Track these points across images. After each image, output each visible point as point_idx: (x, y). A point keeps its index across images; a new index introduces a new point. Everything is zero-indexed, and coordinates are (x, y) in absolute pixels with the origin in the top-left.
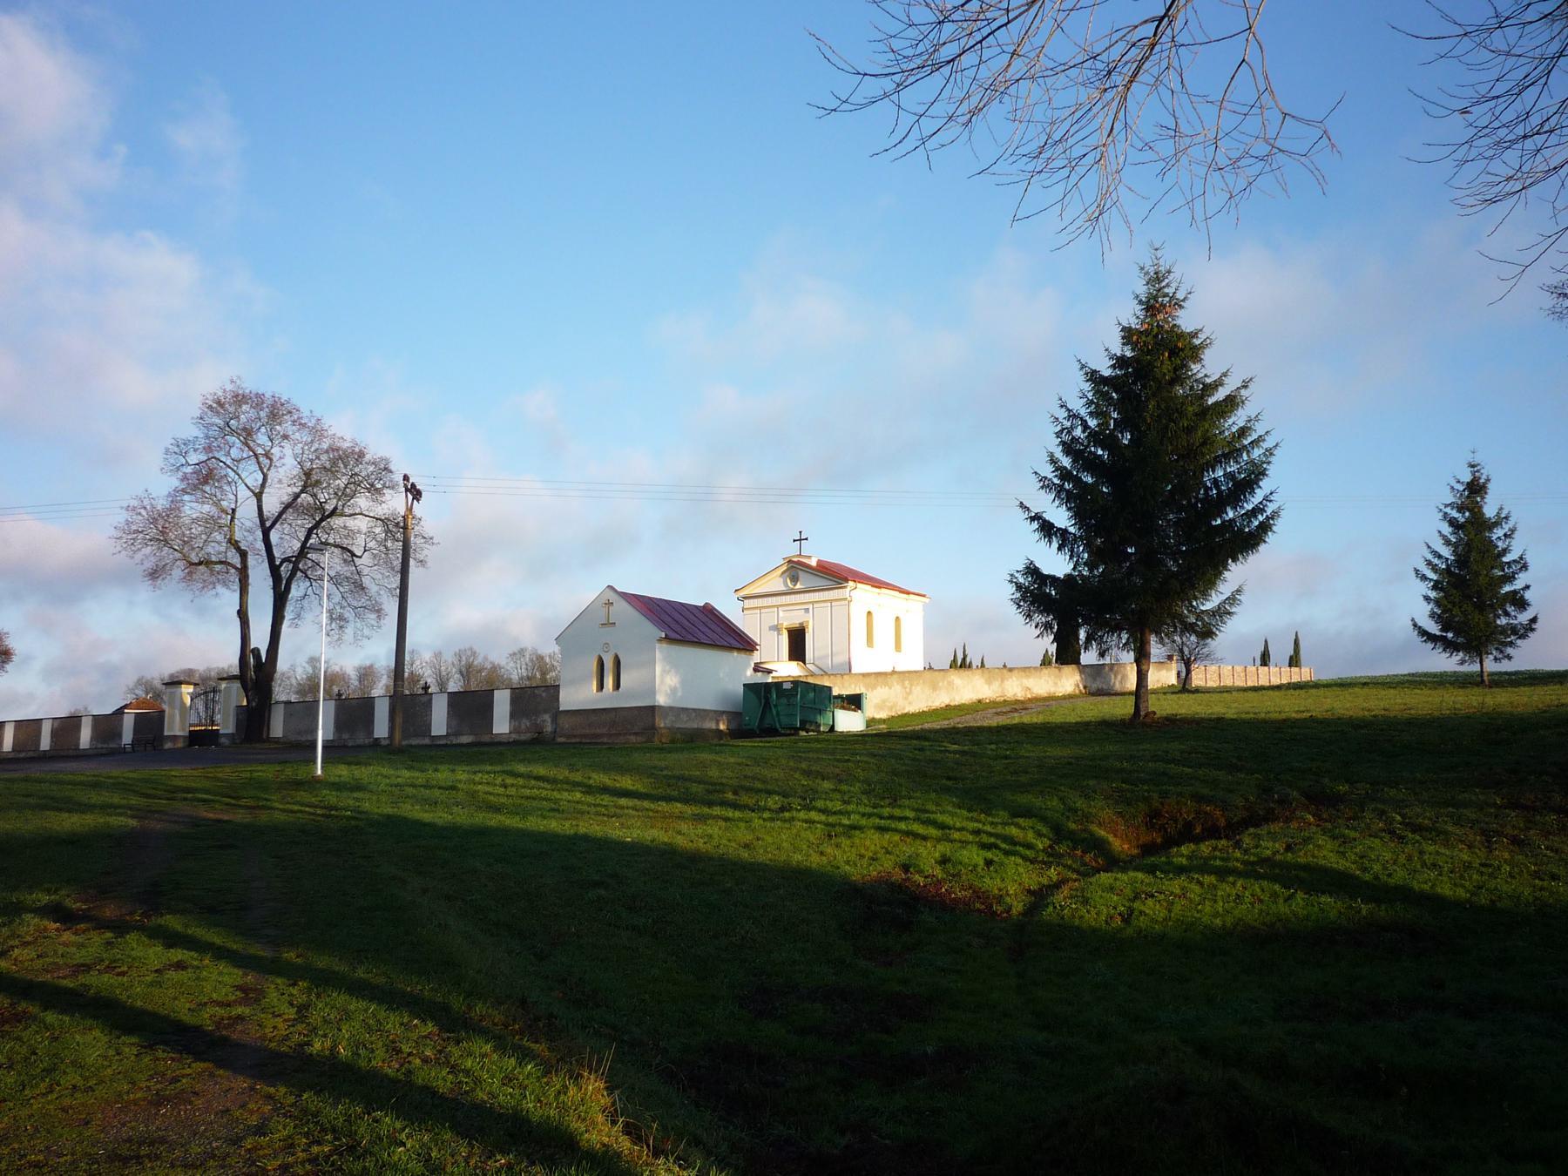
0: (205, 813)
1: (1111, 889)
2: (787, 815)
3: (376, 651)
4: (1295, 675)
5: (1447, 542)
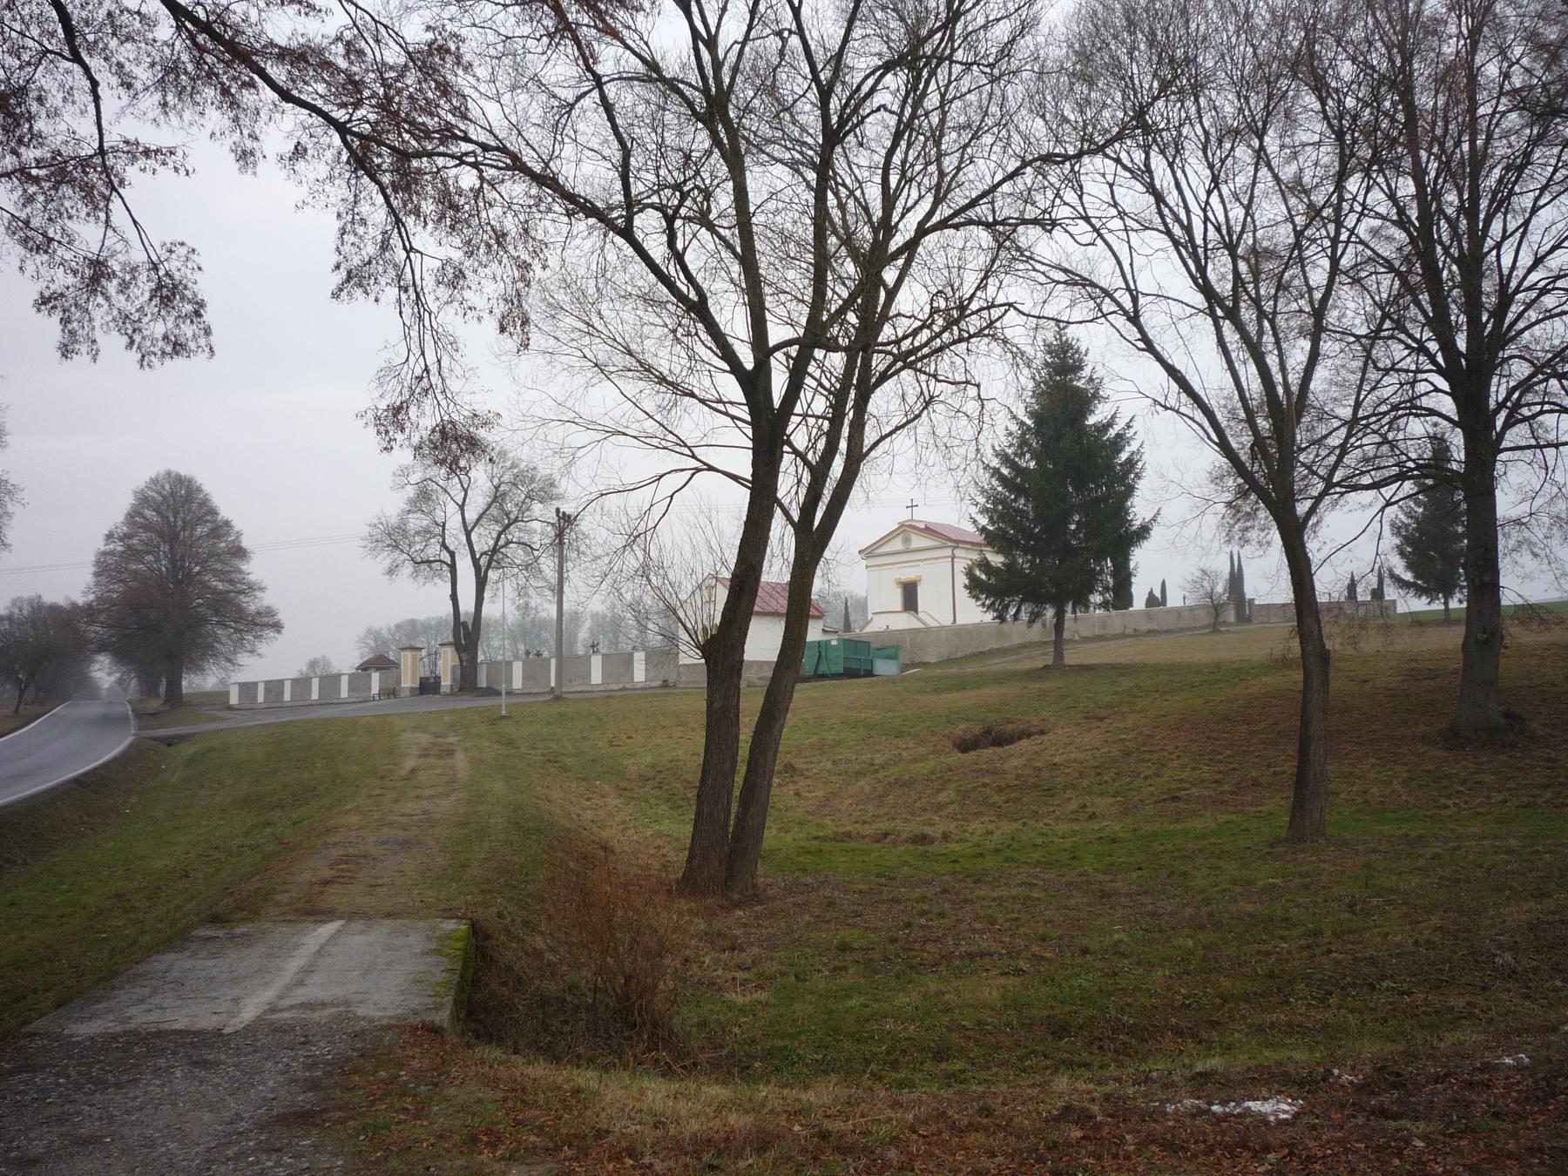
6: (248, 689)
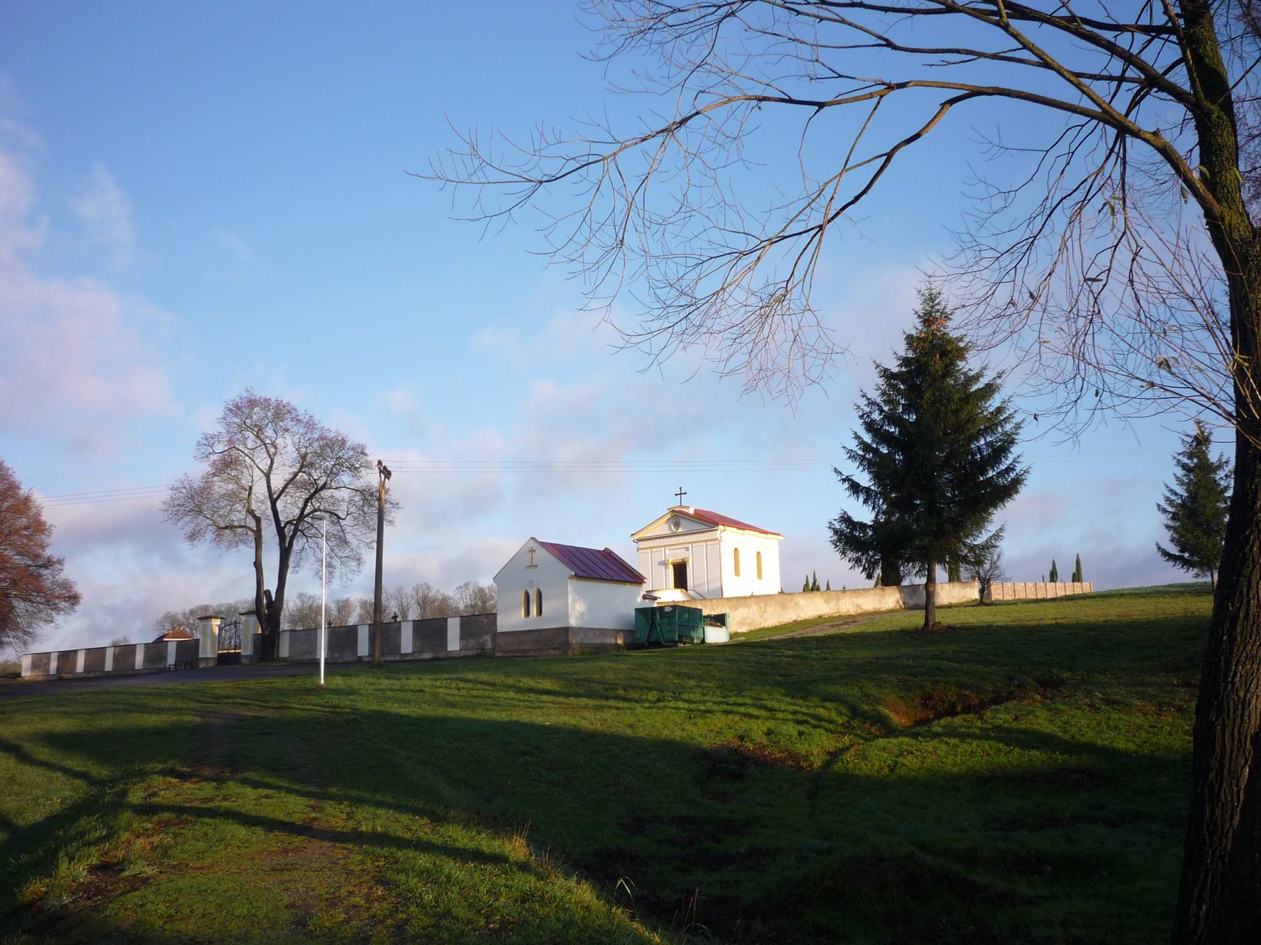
0: (244, 712)
1: (884, 749)
2: (661, 704)
3: (358, 590)
4: (1078, 589)
5: (1181, 483)
6: (40, 661)
